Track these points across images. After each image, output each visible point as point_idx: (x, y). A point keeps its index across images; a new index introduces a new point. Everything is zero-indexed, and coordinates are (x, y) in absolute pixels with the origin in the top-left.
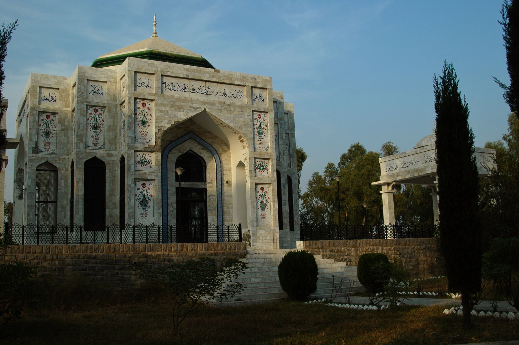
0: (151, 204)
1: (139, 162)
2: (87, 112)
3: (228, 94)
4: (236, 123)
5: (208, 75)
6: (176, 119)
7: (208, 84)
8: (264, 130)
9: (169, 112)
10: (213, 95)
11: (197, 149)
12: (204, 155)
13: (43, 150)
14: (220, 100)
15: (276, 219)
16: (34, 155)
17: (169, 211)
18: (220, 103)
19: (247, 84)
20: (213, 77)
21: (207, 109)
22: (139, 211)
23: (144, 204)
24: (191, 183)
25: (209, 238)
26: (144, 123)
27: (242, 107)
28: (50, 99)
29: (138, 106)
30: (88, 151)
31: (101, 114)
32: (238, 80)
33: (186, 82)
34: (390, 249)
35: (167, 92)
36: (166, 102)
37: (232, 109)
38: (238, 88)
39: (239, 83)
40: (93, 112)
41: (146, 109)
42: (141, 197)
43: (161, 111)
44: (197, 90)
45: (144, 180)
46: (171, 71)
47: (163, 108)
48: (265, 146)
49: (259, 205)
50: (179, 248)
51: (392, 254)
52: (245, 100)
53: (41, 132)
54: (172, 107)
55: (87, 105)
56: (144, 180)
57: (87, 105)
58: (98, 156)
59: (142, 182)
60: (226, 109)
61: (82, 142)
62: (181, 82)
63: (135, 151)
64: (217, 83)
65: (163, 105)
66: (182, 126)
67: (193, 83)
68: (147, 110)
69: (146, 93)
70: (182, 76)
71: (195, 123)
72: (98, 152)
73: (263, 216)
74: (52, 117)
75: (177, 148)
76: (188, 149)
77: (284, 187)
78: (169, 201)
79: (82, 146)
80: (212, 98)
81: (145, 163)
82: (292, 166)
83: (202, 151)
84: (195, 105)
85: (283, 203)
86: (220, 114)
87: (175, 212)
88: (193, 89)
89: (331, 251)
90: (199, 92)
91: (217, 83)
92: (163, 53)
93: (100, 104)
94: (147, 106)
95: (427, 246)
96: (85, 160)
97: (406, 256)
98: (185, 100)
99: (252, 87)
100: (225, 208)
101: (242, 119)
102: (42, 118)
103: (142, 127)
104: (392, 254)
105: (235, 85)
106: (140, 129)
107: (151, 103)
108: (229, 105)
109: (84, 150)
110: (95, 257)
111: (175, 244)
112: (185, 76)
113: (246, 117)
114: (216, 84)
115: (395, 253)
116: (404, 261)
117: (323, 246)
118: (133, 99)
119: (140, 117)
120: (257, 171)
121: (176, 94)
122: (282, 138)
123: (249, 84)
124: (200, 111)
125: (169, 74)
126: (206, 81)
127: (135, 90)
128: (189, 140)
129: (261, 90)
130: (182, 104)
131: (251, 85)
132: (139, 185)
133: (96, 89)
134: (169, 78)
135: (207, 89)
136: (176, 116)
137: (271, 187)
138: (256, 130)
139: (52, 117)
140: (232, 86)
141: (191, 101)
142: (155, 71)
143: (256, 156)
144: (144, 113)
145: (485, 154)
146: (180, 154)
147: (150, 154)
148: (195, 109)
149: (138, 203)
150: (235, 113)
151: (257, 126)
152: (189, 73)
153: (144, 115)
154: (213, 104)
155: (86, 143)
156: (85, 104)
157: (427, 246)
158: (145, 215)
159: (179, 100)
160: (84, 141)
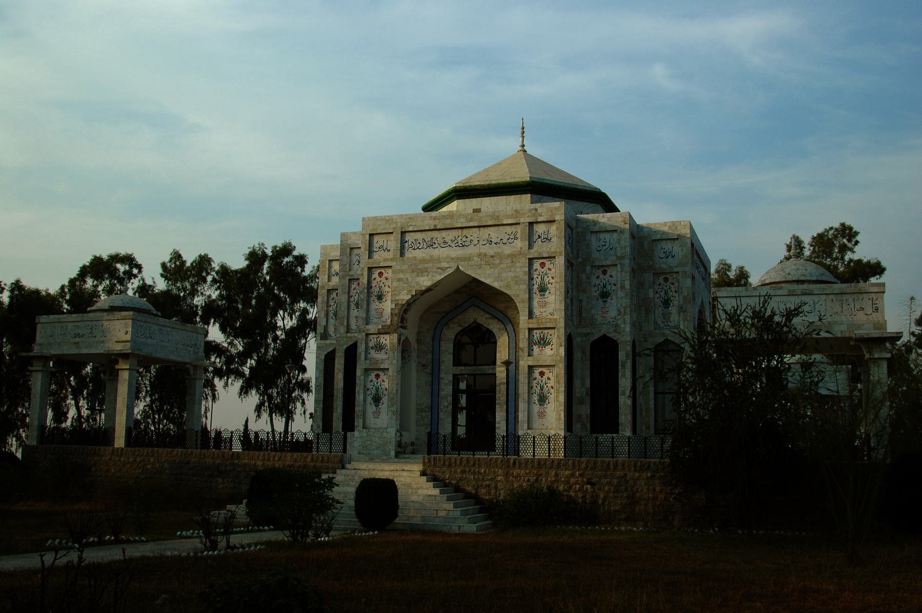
0: (385, 400)
1: (372, 348)
2: (349, 287)
3: (494, 240)
4: (502, 281)
5: (463, 220)
6: (418, 288)
7: (465, 232)
8: (549, 286)
9: (410, 279)
10: (472, 246)
11: (484, 320)
12: (494, 326)
13: (333, 334)
14: (483, 251)
15: (560, 419)
16: (322, 342)
19: (522, 220)
20: (471, 220)
22: (371, 409)
23: (377, 400)
24: (39, 396)
26: (380, 297)
27: (512, 256)
29: (374, 276)
30: (349, 335)
31: (550, 269)
32: (508, 217)
33: (435, 234)
34: (573, 475)
35: (410, 254)
36: (406, 267)
37: (497, 261)
38: (509, 229)
39: (510, 221)
41: (383, 279)
42: (374, 391)
43: (399, 280)
44: (450, 243)
45: (380, 370)
47: (401, 276)
48: (550, 308)
49: (535, 398)
50: (266, 457)
51: (576, 483)
52: (520, 244)
53: (331, 314)
54: (413, 272)
56: (380, 370)
59: (376, 372)
60: (487, 263)
61: (342, 324)
62: (428, 236)
63: (367, 335)
64: (479, 227)
65: (402, 271)
67: (444, 234)
68: (385, 281)
69: (381, 259)
73: (542, 415)
74: (548, 264)
76: (472, 320)
77: (624, 366)
79: (342, 330)
80: (472, 250)
81: (379, 347)
83: (490, 321)
84: (444, 265)
85: (620, 392)
86: (479, 271)
87: (450, 407)
88: (445, 242)
89: (463, 472)
90: (453, 245)
91: (479, 227)
92: (480, 185)
94: (385, 275)
96: (345, 347)
97: (607, 488)
98: (432, 259)
101: (512, 274)
102: (332, 296)
103: (377, 303)
104: (576, 483)
106: (375, 305)
107: (390, 271)
108: (492, 257)
109: (345, 335)
110: (188, 463)
111: (199, 450)
112: (432, 228)
113: (518, 270)
114: (477, 229)
115: (583, 481)
116: (602, 496)
117: (450, 465)
118: (366, 269)
119: (375, 290)
120: (535, 348)
121: (419, 254)
123: (526, 220)
124: (450, 271)
125: (411, 229)
126: (462, 228)
127: (370, 257)
129: (548, 224)
132: (372, 376)
134: (413, 234)
135: (464, 239)
136: (417, 283)
137: (555, 370)
138: (536, 287)
139: (548, 264)
140: (501, 228)
141: (439, 260)
144: (381, 284)
145: (844, 297)
146: (460, 329)
147: (387, 337)
149: (369, 399)
150: (502, 266)
151: (537, 281)
152: (436, 222)
153: (380, 287)
154: (469, 259)
155: (348, 325)
156: (348, 278)
158: (377, 414)
159: (423, 261)
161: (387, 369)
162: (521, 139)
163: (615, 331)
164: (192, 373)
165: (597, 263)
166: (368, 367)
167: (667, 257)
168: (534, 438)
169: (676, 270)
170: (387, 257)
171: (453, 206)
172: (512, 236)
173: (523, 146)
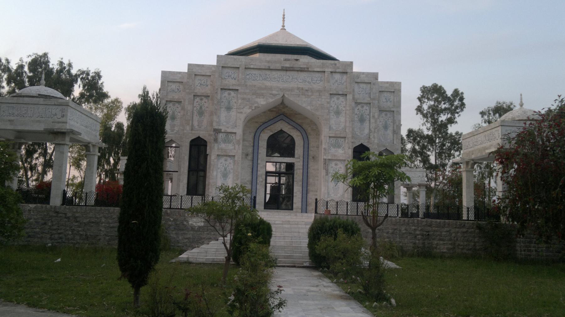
13: (197, 127)
17: (258, 182)
18: (298, 88)
19: (326, 70)
21: (285, 95)
25: (294, 206)
28: (176, 91)
30: (193, 132)
31: (205, 102)
37: (310, 94)
39: (318, 70)
40: (199, 101)
42: (223, 169)
46: (254, 63)
47: (245, 96)
53: (195, 113)
54: (253, 94)
55: (194, 96)
57: (194, 96)
58: (201, 136)
66: (274, 109)
70: (264, 68)
71: (287, 107)
72: (202, 132)
75: (269, 128)
78: (259, 173)
82: (395, 143)
84: (274, 92)
93: (205, 94)
95: (470, 230)
99: (331, 72)
100: (311, 180)
101: (319, 103)
105: (314, 71)
108: (307, 90)
112: (267, 68)
122: (374, 117)
125: (252, 67)
128: (280, 122)
130: (263, 92)
131: (330, 70)
133: (203, 82)
135: (288, 77)
142: (240, 65)
143: (331, 135)
146: (272, 133)
148: (275, 95)
150: (313, 97)
154: (292, 90)
155: (192, 125)
156: (193, 94)
157: (470, 230)
160: (191, 125)
161: (234, 156)
162: (282, 22)
163: (368, 142)
164: (91, 150)
165: (358, 101)
166: (220, 153)
167: (387, 102)
168: (87, 194)
169: (392, 109)
170: (234, 83)
171: (257, 55)
172: (319, 79)
173: (283, 26)
